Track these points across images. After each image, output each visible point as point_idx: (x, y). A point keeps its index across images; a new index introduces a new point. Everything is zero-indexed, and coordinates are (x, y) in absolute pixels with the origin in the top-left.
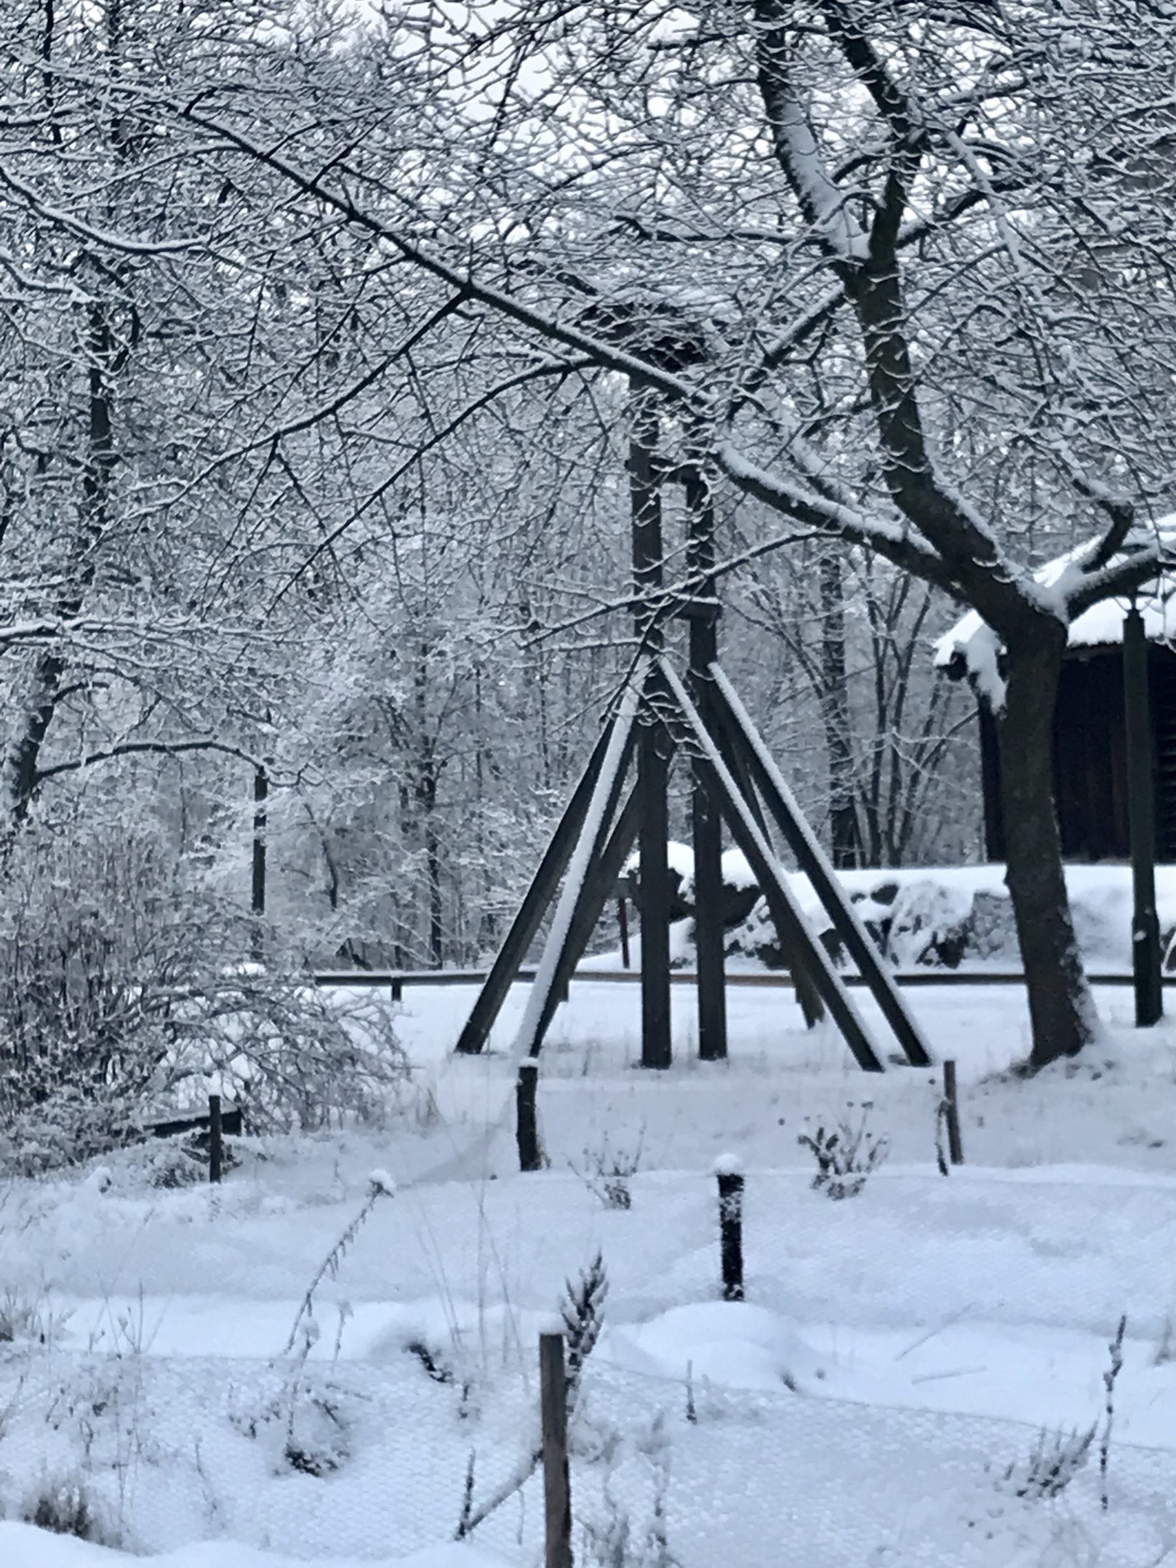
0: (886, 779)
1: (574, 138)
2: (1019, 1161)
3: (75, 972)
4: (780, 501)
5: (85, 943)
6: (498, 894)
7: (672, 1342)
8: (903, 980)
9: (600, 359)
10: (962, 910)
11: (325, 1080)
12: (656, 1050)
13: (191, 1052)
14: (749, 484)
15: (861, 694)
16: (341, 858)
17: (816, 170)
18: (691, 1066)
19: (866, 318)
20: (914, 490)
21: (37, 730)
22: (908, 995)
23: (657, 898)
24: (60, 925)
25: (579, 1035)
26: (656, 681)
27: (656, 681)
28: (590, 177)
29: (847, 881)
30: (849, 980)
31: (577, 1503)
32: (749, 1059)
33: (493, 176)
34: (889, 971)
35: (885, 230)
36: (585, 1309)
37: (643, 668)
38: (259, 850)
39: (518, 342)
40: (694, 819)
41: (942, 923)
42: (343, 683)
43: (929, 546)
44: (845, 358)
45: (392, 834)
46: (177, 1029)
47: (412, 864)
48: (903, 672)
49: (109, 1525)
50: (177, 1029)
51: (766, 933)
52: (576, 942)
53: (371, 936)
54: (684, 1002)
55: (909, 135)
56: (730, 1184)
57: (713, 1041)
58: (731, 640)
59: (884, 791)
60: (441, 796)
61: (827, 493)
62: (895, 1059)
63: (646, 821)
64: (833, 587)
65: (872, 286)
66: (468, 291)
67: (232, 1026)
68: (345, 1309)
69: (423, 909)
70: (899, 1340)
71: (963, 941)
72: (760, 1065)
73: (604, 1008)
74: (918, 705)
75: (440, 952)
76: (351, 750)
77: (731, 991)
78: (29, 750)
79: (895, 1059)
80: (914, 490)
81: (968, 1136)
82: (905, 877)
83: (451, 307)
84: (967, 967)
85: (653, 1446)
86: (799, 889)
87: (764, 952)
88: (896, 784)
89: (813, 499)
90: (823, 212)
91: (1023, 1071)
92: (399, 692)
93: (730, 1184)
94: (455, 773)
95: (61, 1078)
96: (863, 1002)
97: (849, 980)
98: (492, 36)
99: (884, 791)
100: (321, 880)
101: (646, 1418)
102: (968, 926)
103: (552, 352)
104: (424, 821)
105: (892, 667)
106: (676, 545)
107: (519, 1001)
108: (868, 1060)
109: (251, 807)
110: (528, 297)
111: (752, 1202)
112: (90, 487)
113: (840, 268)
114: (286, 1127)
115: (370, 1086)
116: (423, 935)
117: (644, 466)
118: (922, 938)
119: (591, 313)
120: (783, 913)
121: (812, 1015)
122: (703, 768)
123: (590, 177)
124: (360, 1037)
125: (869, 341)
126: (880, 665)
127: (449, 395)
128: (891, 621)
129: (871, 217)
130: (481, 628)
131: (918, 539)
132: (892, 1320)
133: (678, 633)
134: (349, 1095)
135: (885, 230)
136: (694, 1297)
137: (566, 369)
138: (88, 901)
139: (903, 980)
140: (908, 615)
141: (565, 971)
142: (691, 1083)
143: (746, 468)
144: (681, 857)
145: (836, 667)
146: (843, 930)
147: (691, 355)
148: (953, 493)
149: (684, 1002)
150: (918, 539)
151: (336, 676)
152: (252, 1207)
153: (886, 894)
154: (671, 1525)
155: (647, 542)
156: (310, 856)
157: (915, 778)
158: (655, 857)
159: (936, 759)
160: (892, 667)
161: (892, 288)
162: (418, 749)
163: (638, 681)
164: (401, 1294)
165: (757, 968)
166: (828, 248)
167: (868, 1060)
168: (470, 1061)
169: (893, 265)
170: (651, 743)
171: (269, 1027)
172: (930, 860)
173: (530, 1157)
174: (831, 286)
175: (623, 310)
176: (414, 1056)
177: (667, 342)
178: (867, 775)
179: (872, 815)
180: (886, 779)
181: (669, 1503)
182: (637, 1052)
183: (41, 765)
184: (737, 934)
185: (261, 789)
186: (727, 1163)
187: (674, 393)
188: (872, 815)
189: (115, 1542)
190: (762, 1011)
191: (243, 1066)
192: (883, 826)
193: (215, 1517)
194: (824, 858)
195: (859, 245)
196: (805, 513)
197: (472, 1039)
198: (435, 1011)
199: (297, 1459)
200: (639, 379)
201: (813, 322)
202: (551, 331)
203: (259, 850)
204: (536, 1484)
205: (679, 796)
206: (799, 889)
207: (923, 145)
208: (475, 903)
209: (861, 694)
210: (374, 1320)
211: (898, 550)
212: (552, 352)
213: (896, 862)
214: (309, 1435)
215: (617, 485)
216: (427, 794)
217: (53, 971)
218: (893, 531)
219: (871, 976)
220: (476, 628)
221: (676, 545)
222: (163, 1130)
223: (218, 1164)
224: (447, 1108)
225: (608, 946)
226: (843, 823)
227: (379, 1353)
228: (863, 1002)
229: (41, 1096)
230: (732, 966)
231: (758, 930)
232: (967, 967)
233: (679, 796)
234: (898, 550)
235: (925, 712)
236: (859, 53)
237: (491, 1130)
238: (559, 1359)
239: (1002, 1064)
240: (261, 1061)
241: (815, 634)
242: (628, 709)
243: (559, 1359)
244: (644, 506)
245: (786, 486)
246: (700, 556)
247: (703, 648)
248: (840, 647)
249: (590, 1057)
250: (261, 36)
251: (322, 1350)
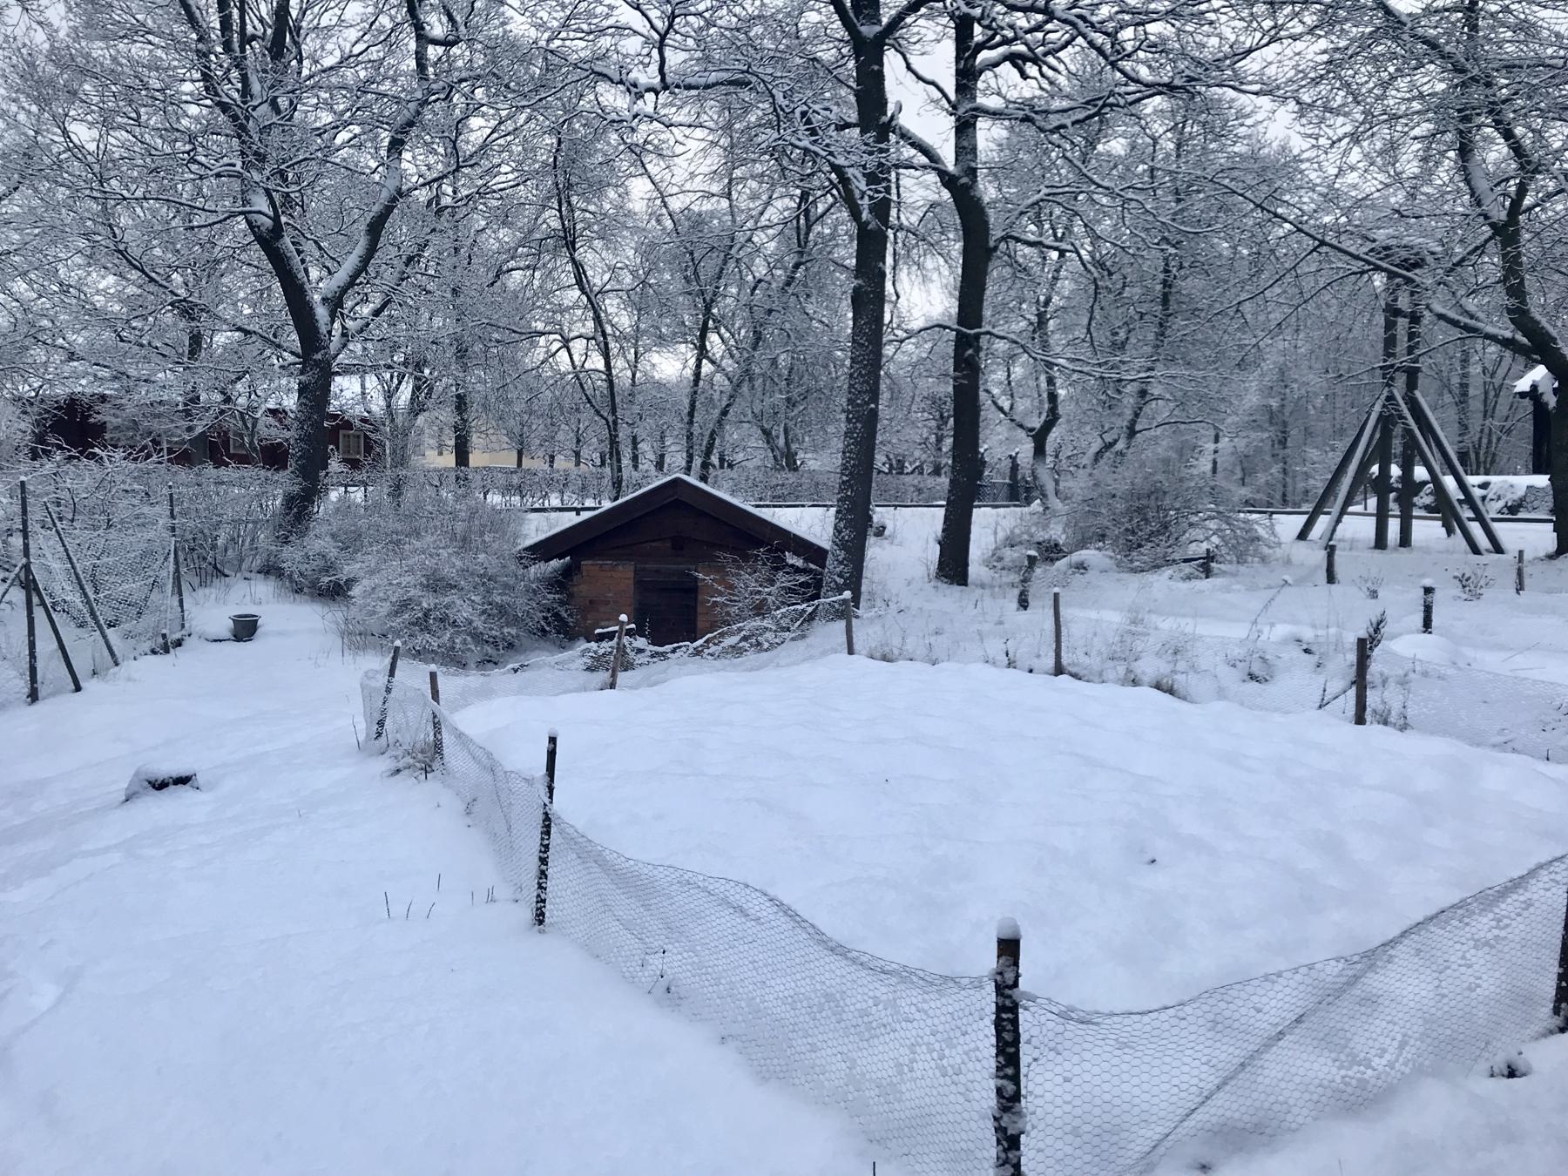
0: (1485, 441)
1: (1363, 181)
2: (1550, 591)
3: (1152, 503)
4: (1455, 323)
5: (1156, 492)
6: (1312, 482)
7: (1405, 645)
8: (1494, 520)
9: (1378, 268)
10: (1521, 493)
11: (1246, 548)
12: (1380, 542)
13: (1196, 533)
14: (1441, 317)
15: (1476, 405)
16: (1246, 467)
17: (1482, 185)
18: (1395, 549)
19: (1504, 245)
20: (1520, 317)
21: (1137, 415)
22: (1496, 526)
23: (1381, 486)
24: (1147, 487)
25: (1348, 535)
26: (1391, 398)
27: (1391, 398)
28: (1377, 195)
29: (1473, 480)
30: (1470, 519)
31: (1369, 701)
32: (1421, 548)
33: (1331, 197)
34: (1488, 517)
35: (1515, 208)
36: (1377, 630)
37: (1385, 393)
38: (1215, 463)
39: (1339, 262)
40: (1404, 454)
41: (1511, 498)
42: (1253, 399)
43: (1525, 340)
44: (1491, 263)
45: (1268, 458)
46: (1191, 525)
47: (1275, 469)
48: (1497, 396)
49: (1182, 692)
50: (1191, 525)
51: (1428, 500)
52: (1349, 501)
53: (1258, 496)
54: (1394, 526)
55: (1527, 163)
56: (1428, 591)
57: (1405, 540)
58: (1422, 380)
59: (1484, 445)
60: (1289, 444)
61: (1472, 317)
62: (1488, 551)
63: (1381, 453)
64: (1465, 361)
65: (1506, 233)
66: (1323, 243)
67: (1212, 525)
68: (1272, 625)
69: (1279, 486)
70: (1503, 655)
71: (1520, 505)
72: (1426, 550)
73: (1359, 526)
74: (1502, 409)
75: (1286, 503)
76: (1254, 425)
77: (1414, 522)
78: (1133, 423)
79: (1488, 551)
80: (1520, 317)
81: (1527, 581)
82: (1492, 479)
83: (1315, 250)
84: (1520, 516)
85: (1403, 682)
86: (1449, 482)
87: (1427, 508)
88: (1490, 442)
89: (1465, 320)
90: (1486, 201)
91: (1551, 557)
92: (1274, 403)
93: (1428, 591)
94: (1294, 433)
95: (1148, 540)
96: (1475, 528)
97: (1470, 519)
98: (1340, 140)
99: (1484, 445)
100: (1239, 475)
101: (1401, 672)
102: (1523, 499)
103: (1357, 266)
104: (1281, 453)
105: (1492, 393)
106: (1403, 343)
107: (1323, 522)
108: (1476, 550)
109: (1212, 446)
110: (1347, 244)
111: (1438, 599)
112: (1161, 325)
113: (1493, 225)
114: (1231, 562)
115: (1266, 550)
116: (1278, 496)
117: (1393, 312)
118: (1501, 504)
119: (1372, 250)
120: (1440, 490)
121: (1450, 532)
122: (1408, 432)
123: (1377, 195)
124: (1261, 532)
125: (1504, 256)
126: (1486, 393)
127: (1308, 284)
128: (1493, 375)
129: (1507, 204)
130: (1313, 378)
131: (1519, 337)
132: (1501, 647)
133: (1401, 380)
134: (1256, 553)
135: (1515, 208)
136: (1410, 632)
137: (1362, 273)
138: (1159, 477)
139: (1494, 520)
140: (1501, 372)
141: (1343, 512)
142: (1394, 557)
143: (1439, 309)
144: (1395, 471)
145: (1465, 394)
146: (1469, 500)
147: (1416, 265)
148: (1538, 317)
149: (1394, 526)
150: (1519, 337)
151: (1251, 394)
152: (1228, 590)
153: (1484, 486)
154: (1409, 712)
155: (1390, 342)
156: (1234, 465)
157: (1499, 439)
158: (1385, 471)
159: (1509, 432)
160: (1492, 393)
161: (1517, 233)
162: (1281, 426)
163: (1383, 397)
164: (1295, 622)
165: (1423, 513)
166: (1486, 217)
167: (1476, 550)
168: (1302, 543)
169: (1517, 223)
170: (1386, 422)
171: (1224, 526)
172: (1501, 473)
173: (1331, 578)
174: (1487, 231)
175: (1387, 248)
176: (1283, 540)
177: (1406, 260)
178: (1476, 439)
179: (1477, 454)
180: (1485, 441)
181: (1409, 704)
182: (1373, 543)
183: (1138, 428)
184: (1415, 499)
185: (1217, 440)
186: (1428, 582)
187: (1409, 281)
188: (1477, 454)
189: (1184, 699)
190: (1427, 530)
191: (1215, 539)
192: (1482, 458)
193: (1221, 694)
194: (1460, 469)
195: (1503, 215)
196: (1466, 328)
197: (1303, 535)
198: (1290, 524)
199: (1252, 677)
200: (1391, 275)
201: (1477, 248)
202: (1357, 258)
203: (1215, 463)
204: (1352, 692)
205: (1397, 446)
206: (1449, 482)
207: (1536, 171)
208: (1301, 485)
209: (1476, 405)
210: (1282, 630)
211: (1507, 343)
212: (1357, 266)
213: (1487, 473)
214: (1257, 669)
215: (1380, 319)
216: (1283, 443)
217: (1144, 502)
218: (1508, 334)
219: (1479, 518)
220: (1312, 380)
221: (1403, 343)
222: (1186, 561)
223: (1208, 573)
224: (1294, 559)
225: (1358, 503)
226: (1463, 457)
227: (1284, 642)
228: (1475, 528)
229: (1140, 546)
230: (1416, 512)
231: (1424, 498)
232: (1520, 516)
233: (1397, 446)
234: (1507, 343)
235: (1505, 413)
236: (1508, 135)
237: (1317, 567)
238: (1364, 649)
239: (1542, 554)
240: (1222, 538)
241: (1455, 380)
242: (1377, 408)
243: (1364, 649)
244: (1390, 325)
245: (1457, 317)
246: (1410, 350)
247: (1412, 384)
248: (1467, 385)
249: (1353, 544)
250: (1236, 149)
251: (1263, 637)
